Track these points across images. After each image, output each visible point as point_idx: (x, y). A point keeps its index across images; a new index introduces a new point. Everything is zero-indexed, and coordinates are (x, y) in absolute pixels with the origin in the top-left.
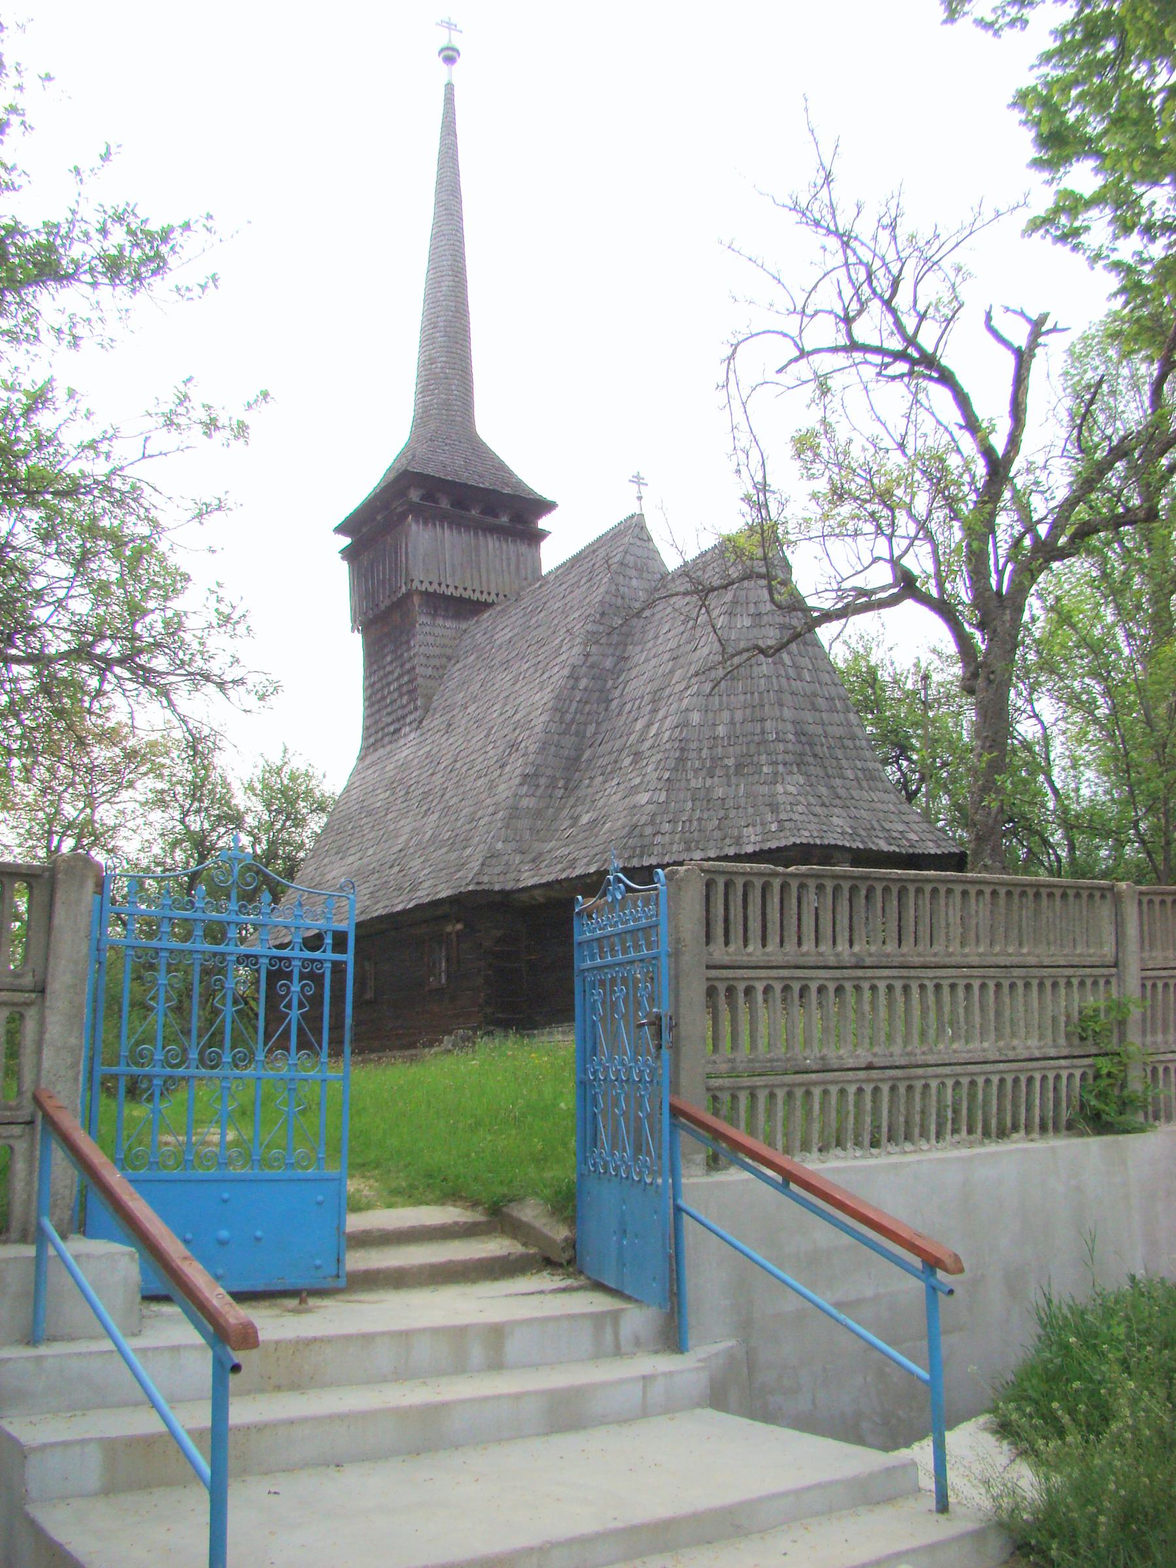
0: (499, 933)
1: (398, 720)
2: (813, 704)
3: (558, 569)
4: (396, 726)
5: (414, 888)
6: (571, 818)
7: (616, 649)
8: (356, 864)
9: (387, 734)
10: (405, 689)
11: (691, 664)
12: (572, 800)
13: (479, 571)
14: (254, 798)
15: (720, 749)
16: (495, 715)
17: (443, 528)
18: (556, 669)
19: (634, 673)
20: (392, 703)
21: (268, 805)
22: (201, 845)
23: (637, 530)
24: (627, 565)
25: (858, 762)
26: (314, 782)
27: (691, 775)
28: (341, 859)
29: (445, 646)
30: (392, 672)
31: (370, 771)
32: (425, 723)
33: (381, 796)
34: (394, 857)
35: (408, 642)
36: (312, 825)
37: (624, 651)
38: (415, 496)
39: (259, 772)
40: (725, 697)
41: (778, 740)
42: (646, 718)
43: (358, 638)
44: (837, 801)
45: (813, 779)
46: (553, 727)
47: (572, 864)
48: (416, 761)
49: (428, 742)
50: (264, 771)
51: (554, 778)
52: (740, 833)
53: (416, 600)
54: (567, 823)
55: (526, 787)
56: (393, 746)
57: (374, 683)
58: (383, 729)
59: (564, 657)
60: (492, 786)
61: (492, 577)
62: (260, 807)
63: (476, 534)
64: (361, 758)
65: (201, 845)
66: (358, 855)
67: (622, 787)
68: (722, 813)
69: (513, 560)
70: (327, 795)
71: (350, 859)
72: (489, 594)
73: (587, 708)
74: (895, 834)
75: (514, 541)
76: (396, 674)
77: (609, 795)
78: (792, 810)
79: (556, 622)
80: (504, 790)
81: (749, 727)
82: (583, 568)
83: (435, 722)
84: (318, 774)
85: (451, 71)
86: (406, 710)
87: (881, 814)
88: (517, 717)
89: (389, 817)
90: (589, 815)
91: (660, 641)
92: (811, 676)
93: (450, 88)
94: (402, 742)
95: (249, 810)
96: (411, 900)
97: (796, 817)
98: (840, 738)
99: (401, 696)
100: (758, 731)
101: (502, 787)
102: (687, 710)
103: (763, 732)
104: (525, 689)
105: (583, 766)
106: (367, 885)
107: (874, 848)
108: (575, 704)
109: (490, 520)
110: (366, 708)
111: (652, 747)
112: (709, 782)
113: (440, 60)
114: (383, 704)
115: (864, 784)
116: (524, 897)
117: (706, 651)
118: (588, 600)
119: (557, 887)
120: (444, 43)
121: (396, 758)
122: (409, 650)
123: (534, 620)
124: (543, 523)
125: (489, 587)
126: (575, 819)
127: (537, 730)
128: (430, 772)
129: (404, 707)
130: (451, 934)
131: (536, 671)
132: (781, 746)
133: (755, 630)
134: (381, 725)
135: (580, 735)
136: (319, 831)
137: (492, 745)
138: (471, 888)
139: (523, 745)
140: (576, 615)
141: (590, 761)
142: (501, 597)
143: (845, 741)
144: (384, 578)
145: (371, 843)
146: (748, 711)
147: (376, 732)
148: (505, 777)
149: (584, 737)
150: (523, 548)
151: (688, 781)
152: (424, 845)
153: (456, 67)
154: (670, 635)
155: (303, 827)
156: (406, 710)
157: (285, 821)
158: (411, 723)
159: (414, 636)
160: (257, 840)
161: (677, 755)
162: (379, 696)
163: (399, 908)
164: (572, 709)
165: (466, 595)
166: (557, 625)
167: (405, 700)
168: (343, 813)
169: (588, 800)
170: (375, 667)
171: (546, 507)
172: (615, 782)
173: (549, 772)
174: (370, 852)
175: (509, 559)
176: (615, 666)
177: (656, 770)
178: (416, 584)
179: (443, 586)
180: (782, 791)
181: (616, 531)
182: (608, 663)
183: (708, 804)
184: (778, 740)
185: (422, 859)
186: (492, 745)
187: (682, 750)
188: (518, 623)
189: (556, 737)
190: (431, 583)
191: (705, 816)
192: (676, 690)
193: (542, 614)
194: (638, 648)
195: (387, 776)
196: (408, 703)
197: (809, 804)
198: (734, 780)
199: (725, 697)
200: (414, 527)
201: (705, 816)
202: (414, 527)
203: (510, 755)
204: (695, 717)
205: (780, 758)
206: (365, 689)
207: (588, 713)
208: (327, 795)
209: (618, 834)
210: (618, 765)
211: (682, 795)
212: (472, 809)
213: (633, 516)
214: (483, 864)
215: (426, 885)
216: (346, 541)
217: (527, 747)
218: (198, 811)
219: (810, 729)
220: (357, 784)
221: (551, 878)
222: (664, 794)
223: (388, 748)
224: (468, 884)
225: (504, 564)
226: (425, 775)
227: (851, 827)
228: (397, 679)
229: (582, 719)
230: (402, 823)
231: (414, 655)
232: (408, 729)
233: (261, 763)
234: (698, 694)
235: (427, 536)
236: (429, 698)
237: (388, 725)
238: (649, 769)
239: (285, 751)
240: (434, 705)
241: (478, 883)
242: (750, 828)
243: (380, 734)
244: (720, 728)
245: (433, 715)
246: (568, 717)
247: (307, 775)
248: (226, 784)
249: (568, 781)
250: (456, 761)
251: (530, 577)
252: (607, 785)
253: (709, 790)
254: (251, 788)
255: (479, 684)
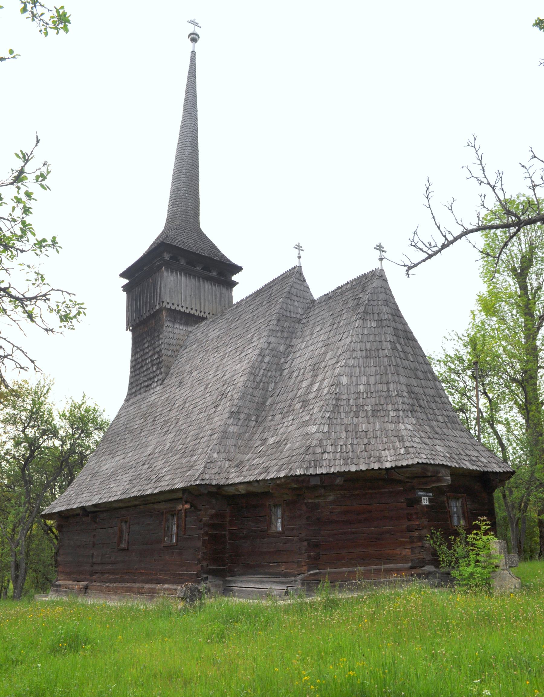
0: (213, 512)
1: (150, 379)
2: (415, 374)
3: (247, 298)
4: (149, 382)
5: (158, 480)
6: (261, 440)
7: (286, 340)
8: (121, 461)
9: (143, 387)
10: (155, 362)
11: (338, 348)
12: (261, 429)
13: (200, 299)
14: (64, 421)
15: (361, 400)
16: (210, 377)
17: (181, 275)
18: (250, 351)
19: (298, 354)
20: (147, 370)
21: (72, 426)
22: (33, 444)
23: (298, 275)
24: (292, 294)
25: (444, 412)
26: (98, 413)
27: (343, 415)
28: (112, 458)
29: (179, 339)
30: (148, 352)
31: (132, 408)
32: (165, 381)
33: (138, 422)
34: (145, 459)
35: (159, 336)
36: (95, 436)
37: (291, 342)
38: (167, 256)
39: (68, 408)
40: (362, 368)
41: (398, 395)
42: (310, 380)
43: (129, 334)
44: (436, 436)
45: (421, 421)
46: (249, 384)
47: (267, 470)
48: (160, 402)
49: (168, 392)
50: (72, 406)
51: (249, 416)
52: (380, 454)
53: (164, 313)
54: (259, 443)
55: (232, 419)
56: (147, 394)
57: (137, 359)
58: (141, 384)
59: (254, 344)
60: (209, 418)
61: (207, 303)
62: (68, 426)
63: (199, 280)
64: (127, 400)
65: (33, 444)
66: (123, 456)
67: (296, 421)
68: (366, 441)
69: (218, 296)
70: (104, 421)
71: (117, 459)
72: (205, 313)
73: (269, 374)
74: (474, 458)
75: (219, 286)
76: (150, 354)
77: (287, 426)
78: (412, 441)
79: (248, 325)
80: (218, 421)
81: (379, 387)
82: (264, 296)
83: (172, 381)
84: (101, 409)
85: (194, 47)
86: (155, 374)
87: (462, 445)
88: (225, 378)
89: (143, 434)
90: (273, 439)
91: (314, 336)
92: (413, 358)
93: (193, 53)
94: (152, 392)
95: (61, 427)
96: (156, 488)
97: (415, 445)
98: (433, 396)
99: (153, 366)
100: (385, 389)
101: (216, 419)
102: (339, 375)
103: (388, 390)
104: (229, 363)
105: (267, 408)
106: (127, 475)
107: (465, 467)
108: (262, 371)
109: (207, 273)
110: (131, 372)
111: (316, 397)
112: (355, 420)
113: (189, 40)
114: (141, 370)
115: (449, 425)
116: (232, 490)
117: (348, 341)
118: (268, 313)
119: (256, 484)
120: (191, 31)
121: (148, 400)
122: (159, 340)
123: (233, 325)
124: (234, 278)
125: (204, 309)
126: (264, 441)
127: (239, 385)
128: (168, 409)
129: (154, 372)
130: (181, 510)
131: (236, 352)
132: (400, 400)
133: (379, 329)
134: (139, 382)
135: (266, 390)
136: (98, 440)
137: (209, 394)
138: (198, 482)
139: (229, 394)
140: (261, 321)
141: (271, 405)
142: (211, 314)
143: (435, 398)
144: (147, 301)
145: (131, 450)
146: (378, 377)
147: (137, 386)
148: (217, 413)
149: (267, 391)
150: (224, 290)
151: (342, 419)
152: (164, 453)
153: (196, 44)
154: (321, 332)
155: (90, 437)
156: (155, 374)
157: (80, 434)
158: (157, 381)
159: (162, 333)
160: (64, 442)
161: (334, 402)
162: (140, 366)
163: (149, 492)
164: (260, 374)
165: (192, 312)
166: (248, 327)
167: (154, 368)
168: (114, 431)
169: (272, 428)
170: (138, 350)
171: (238, 269)
172: (291, 418)
173: (246, 411)
174: (130, 455)
175: (216, 295)
176: (286, 350)
177: (320, 412)
178: (165, 304)
179: (176, 306)
180: (404, 428)
181: (284, 276)
182: (282, 348)
183: (356, 435)
184: (398, 395)
185: (163, 461)
186: (209, 394)
187: (337, 399)
188: (223, 327)
189: (251, 390)
190: (173, 304)
191: (355, 443)
192: (330, 362)
193: (239, 322)
194: (300, 340)
195: (142, 410)
196: (157, 370)
197: (421, 437)
198: (371, 419)
199: (362, 368)
200: (165, 273)
201: (355, 443)
202: (165, 273)
203: (221, 400)
204: (344, 380)
205: (400, 407)
206: (132, 362)
207: (270, 377)
208: (104, 421)
209: (297, 451)
210: (292, 408)
211: (338, 428)
212: (197, 431)
213: (295, 268)
214: (205, 467)
215: (167, 478)
216: (126, 281)
217: (232, 396)
218: (33, 427)
219: (416, 390)
220: (124, 415)
221: (252, 478)
222: (326, 427)
223: (143, 395)
224: (196, 480)
225: (214, 297)
226: (165, 411)
227: (448, 453)
228: (151, 356)
229: (267, 380)
230: (150, 438)
231: (162, 343)
232: (155, 384)
233: (70, 402)
234: (345, 366)
235: (172, 279)
236: (169, 368)
237: (144, 382)
238: (315, 411)
239: (84, 397)
240: (172, 371)
241: (203, 480)
242: (386, 451)
243: (139, 387)
244: (361, 387)
245: (171, 377)
246: (258, 379)
247: (94, 410)
248: (50, 413)
249: (258, 417)
250: (185, 403)
251: (227, 305)
252: (285, 420)
253: (356, 425)
254: (64, 415)
255: (199, 360)
